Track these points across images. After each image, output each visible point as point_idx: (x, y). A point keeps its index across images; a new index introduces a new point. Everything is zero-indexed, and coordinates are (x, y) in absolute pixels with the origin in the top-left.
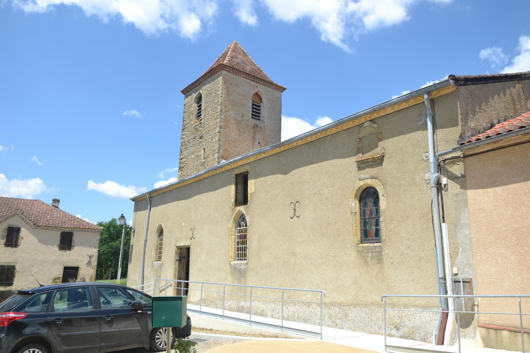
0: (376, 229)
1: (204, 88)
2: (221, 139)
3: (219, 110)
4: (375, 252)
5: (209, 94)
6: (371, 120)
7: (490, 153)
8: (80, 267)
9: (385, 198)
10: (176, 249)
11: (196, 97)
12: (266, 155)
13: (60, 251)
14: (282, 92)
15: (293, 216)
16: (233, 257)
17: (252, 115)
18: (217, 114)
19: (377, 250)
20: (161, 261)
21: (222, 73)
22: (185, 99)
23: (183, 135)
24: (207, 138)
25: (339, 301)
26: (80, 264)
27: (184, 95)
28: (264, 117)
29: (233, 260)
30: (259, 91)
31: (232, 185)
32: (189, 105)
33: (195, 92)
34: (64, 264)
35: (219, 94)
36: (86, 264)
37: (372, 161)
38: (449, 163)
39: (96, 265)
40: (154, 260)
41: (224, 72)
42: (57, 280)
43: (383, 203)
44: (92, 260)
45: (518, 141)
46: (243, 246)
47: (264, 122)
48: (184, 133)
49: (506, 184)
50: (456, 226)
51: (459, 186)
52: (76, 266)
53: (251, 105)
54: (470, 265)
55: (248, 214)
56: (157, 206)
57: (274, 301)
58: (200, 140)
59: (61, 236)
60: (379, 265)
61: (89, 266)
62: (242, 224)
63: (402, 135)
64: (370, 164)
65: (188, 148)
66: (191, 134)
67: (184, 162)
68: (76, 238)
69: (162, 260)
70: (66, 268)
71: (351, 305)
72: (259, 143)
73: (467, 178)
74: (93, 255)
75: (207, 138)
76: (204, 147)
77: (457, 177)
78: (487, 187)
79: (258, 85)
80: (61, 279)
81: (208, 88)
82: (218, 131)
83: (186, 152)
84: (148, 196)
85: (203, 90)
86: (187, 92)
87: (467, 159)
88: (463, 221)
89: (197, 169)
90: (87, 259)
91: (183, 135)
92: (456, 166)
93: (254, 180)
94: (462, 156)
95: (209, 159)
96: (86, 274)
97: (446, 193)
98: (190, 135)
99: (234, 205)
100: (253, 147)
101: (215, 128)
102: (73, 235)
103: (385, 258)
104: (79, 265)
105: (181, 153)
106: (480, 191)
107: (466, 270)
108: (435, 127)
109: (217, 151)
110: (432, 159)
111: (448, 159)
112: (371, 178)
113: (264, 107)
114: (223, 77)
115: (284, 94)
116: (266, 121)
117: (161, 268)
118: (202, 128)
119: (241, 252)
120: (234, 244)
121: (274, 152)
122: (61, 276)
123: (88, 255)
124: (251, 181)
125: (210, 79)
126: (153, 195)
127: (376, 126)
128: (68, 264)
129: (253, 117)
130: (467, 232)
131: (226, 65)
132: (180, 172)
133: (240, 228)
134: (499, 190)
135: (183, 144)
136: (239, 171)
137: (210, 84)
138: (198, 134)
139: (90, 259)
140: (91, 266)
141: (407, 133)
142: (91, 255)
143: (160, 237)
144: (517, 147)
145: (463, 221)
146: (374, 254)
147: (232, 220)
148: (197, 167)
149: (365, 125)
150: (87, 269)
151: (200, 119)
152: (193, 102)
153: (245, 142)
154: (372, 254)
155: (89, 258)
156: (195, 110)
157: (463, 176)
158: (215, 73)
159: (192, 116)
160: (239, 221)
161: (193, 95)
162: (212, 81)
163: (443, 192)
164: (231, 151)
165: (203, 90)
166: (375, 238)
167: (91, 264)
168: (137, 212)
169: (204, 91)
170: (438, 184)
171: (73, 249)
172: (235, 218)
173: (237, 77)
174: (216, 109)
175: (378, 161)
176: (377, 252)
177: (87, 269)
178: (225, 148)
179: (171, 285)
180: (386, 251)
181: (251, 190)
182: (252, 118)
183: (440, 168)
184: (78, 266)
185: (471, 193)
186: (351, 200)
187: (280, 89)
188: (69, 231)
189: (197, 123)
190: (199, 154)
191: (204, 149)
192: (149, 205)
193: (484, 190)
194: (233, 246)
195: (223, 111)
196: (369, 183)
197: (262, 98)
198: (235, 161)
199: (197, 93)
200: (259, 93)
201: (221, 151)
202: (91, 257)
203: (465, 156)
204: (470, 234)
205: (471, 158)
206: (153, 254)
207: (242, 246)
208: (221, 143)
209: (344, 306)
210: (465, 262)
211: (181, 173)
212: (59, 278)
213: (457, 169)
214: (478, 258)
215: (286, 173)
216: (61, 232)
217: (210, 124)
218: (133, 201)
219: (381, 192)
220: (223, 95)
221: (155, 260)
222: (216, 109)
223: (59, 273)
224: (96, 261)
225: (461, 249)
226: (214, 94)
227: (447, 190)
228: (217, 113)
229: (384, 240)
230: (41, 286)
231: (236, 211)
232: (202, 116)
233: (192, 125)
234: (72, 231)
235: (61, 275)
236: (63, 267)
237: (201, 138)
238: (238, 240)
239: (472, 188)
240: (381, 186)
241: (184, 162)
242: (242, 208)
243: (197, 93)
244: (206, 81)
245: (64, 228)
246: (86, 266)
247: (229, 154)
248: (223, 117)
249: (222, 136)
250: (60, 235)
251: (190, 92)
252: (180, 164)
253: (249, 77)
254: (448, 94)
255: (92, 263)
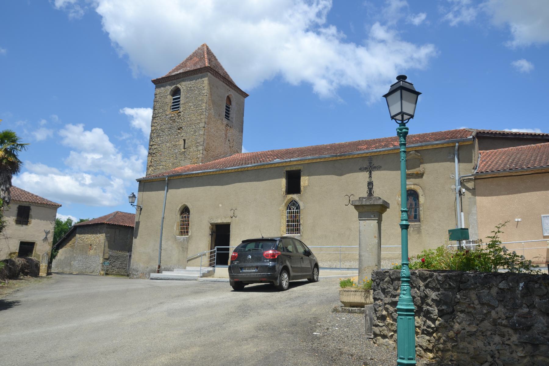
0: (415, 215)
1: (183, 83)
2: (205, 133)
3: (204, 108)
4: (416, 227)
5: (190, 90)
6: (415, 151)
7: (490, 179)
8: (36, 242)
9: (424, 197)
10: (210, 225)
11: (171, 90)
12: (321, 161)
13: (17, 225)
14: (245, 97)
15: (347, 204)
16: (284, 231)
17: (225, 115)
18: (201, 110)
19: (417, 226)
20: (188, 235)
21: (207, 75)
22: (155, 89)
23: (154, 123)
24: (188, 130)
25: (388, 257)
26: (37, 240)
27: (155, 85)
28: (232, 118)
29: (284, 233)
30: (230, 95)
31: (283, 178)
32: (162, 95)
33: (171, 85)
34: (20, 239)
35: (204, 93)
36: (43, 240)
37: (416, 175)
38: (466, 182)
39: (52, 241)
40: (176, 234)
41: (209, 74)
42: (13, 255)
43: (422, 200)
44: (48, 236)
45: (506, 175)
46: (294, 223)
47: (232, 122)
48: (154, 121)
49: (497, 195)
50: (469, 214)
51: (471, 194)
52: (32, 241)
53: (225, 107)
54: (476, 234)
55: (301, 201)
56: (179, 188)
57: (330, 260)
58: (179, 131)
59: (18, 210)
60: (418, 235)
61: (45, 242)
62: (292, 208)
63: (437, 162)
64: (413, 176)
65: (162, 136)
66: (165, 123)
67: (155, 149)
68: (34, 211)
69: (190, 234)
70: (22, 243)
71: (397, 259)
72: (229, 140)
73: (476, 190)
74: (49, 231)
75: (188, 130)
76: (184, 138)
77: (470, 189)
78: (488, 196)
79: (230, 89)
80: (17, 254)
81: (189, 84)
82: (203, 126)
83: (158, 139)
84: (167, 179)
85: (183, 85)
86: (159, 83)
87: (477, 181)
88: (473, 212)
89: (174, 157)
90: (44, 235)
91: (154, 123)
92: (470, 183)
93: (308, 177)
94: (474, 178)
95: (191, 150)
96: (42, 250)
97: (464, 197)
98: (165, 124)
99: (285, 194)
100: (225, 143)
101: (199, 123)
102: (31, 209)
103: (423, 231)
104: (36, 240)
105: (151, 140)
106: (484, 197)
107: (473, 236)
108: (459, 162)
109: (202, 143)
110: (457, 178)
111: (466, 179)
112: (414, 185)
113: (233, 109)
114: (208, 78)
115: (246, 99)
116: (234, 122)
117: (188, 241)
118: (181, 120)
119: (292, 228)
120: (285, 222)
121: (331, 159)
122: (17, 251)
123: (45, 231)
124: (304, 177)
125: (192, 77)
126: (172, 178)
127: (419, 154)
128: (24, 238)
129: (226, 117)
130: (475, 217)
131: (211, 68)
132: (151, 158)
133: (290, 211)
134: (494, 198)
135: (154, 131)
136: (290, 168)
137: (191, 82)
138: (175, 125)
139: (46, 235)
140: (47, 242)
141: (440, 162)
142: (48, 231)
143: (181, 215)
144: (505, 178)
145: (473, 212)
146: (415, 228)
147: (284, 204)
148: (175, 155)
149: (411, 153)
150: (43, 245)
151: (178, 111)
152: (168, 94)
153: (220, 138)
154: (414, 228)
155: (45, 234)
156: (169, 102)
157: (474, 189)
158: (199, 73)
159: (166, 107)
160: (289, 205)
161: (167, 87)
162: (194, 79)
163: (462, 196)
164: (211, 145)
165: (183, 85)
166: (414, 219)
167: (48, 240)
168: (144, 192)
169: (183, 86)
170: (460, 191)
171: (29, 224)
172: (286, 203)
173: (217, 79)
174: (199, 106)
175: (420, 176)
176: (417, 227)
177: (43, 245)
178: (208, 142)
179: (205, 255)
180: (424, 227)
181: (304, 183)
182: (225, 118)
183: (462, 183)
184: (34, 242)
185: (478, 198)
186: (397, 196)
187: (244, 95)
188: (27, 205)
189: (174, 114)
190: (177, 143)
191: (184, 140)
192: (166, 187)
193: (486, 197)
194: (284, 224)
195: (207, 109)
196: (412, 187)
197: (231, 100)
198: (291, 161)
199: (174, 86)
200: (230, 97)
201: (205, 144)
202: (47, 233)
203: (475, 179)
204: (477, 218)
205: (479, 180)
206: (175, 229)
207: (292, 224)
208: (205, 137)
209: (392, 259)
210: (473, 232)
211: (152, 159)
212: (14, 253)
213: (470, 185)
214: (481, 230)
215: (341, 175)
216: (18, 205)
217: (193, 118)
218: (138, 181)
219: (420, 192)
220: (208, 95)
221: (177, 234)
222: (199, 106)
223: (15, 247)
224: (52, 238)
225: (471, 226)
226: (196, 92)
227: (464, 195)
228: (201, 109)
229: (422, 221)
230: (263, 237)
231: (288, 198)
232: (181, 109)
233: (167, 115)
234: (29, 205)
235: (16, 250)
236: (20, 241)
237: (179, 129)
238: (288, 219)
239: (478, 196)
240: (421, 190)
241: (155, 149)
242: (295, 197)
243: (174, 86)
244: (186, 78)
245: (21, 203)
246: (43, 242)
247: (210, 148)
248: (207, 114)
249: (206, 131)
250: (17, 209)
251: (163, 84)
252: (149, 149)
253: (226, 81)
254: (467, 145)
255: (48, 239)
